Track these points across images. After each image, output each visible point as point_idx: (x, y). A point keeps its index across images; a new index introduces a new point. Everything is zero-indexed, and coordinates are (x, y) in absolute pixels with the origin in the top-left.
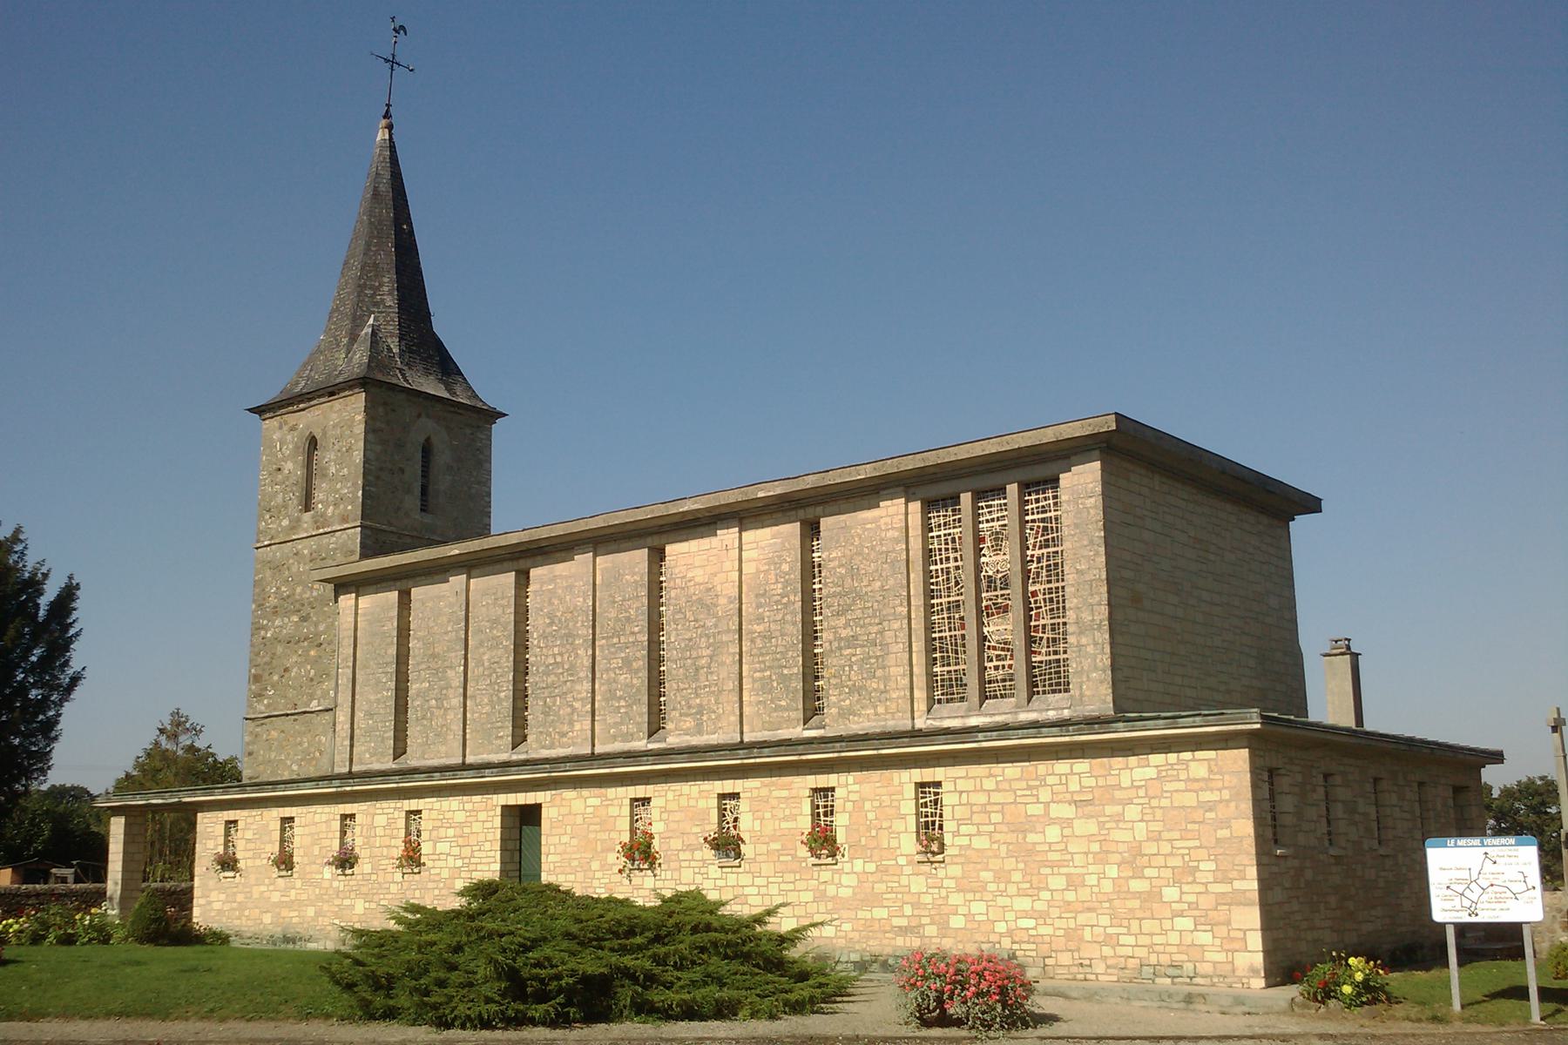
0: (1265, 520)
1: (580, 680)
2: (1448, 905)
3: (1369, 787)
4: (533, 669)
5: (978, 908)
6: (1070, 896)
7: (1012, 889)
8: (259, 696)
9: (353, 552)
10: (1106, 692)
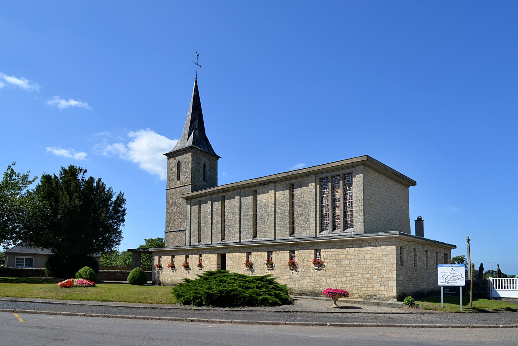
0: (402, 186)
1: (237, 224)
2: (442, 281)
3: (425, 253)
4: (226, 221)
5: (329, 280)
6: (351, 278)
7: (337, 276)
8: (168, 226)
10: (362, 228)
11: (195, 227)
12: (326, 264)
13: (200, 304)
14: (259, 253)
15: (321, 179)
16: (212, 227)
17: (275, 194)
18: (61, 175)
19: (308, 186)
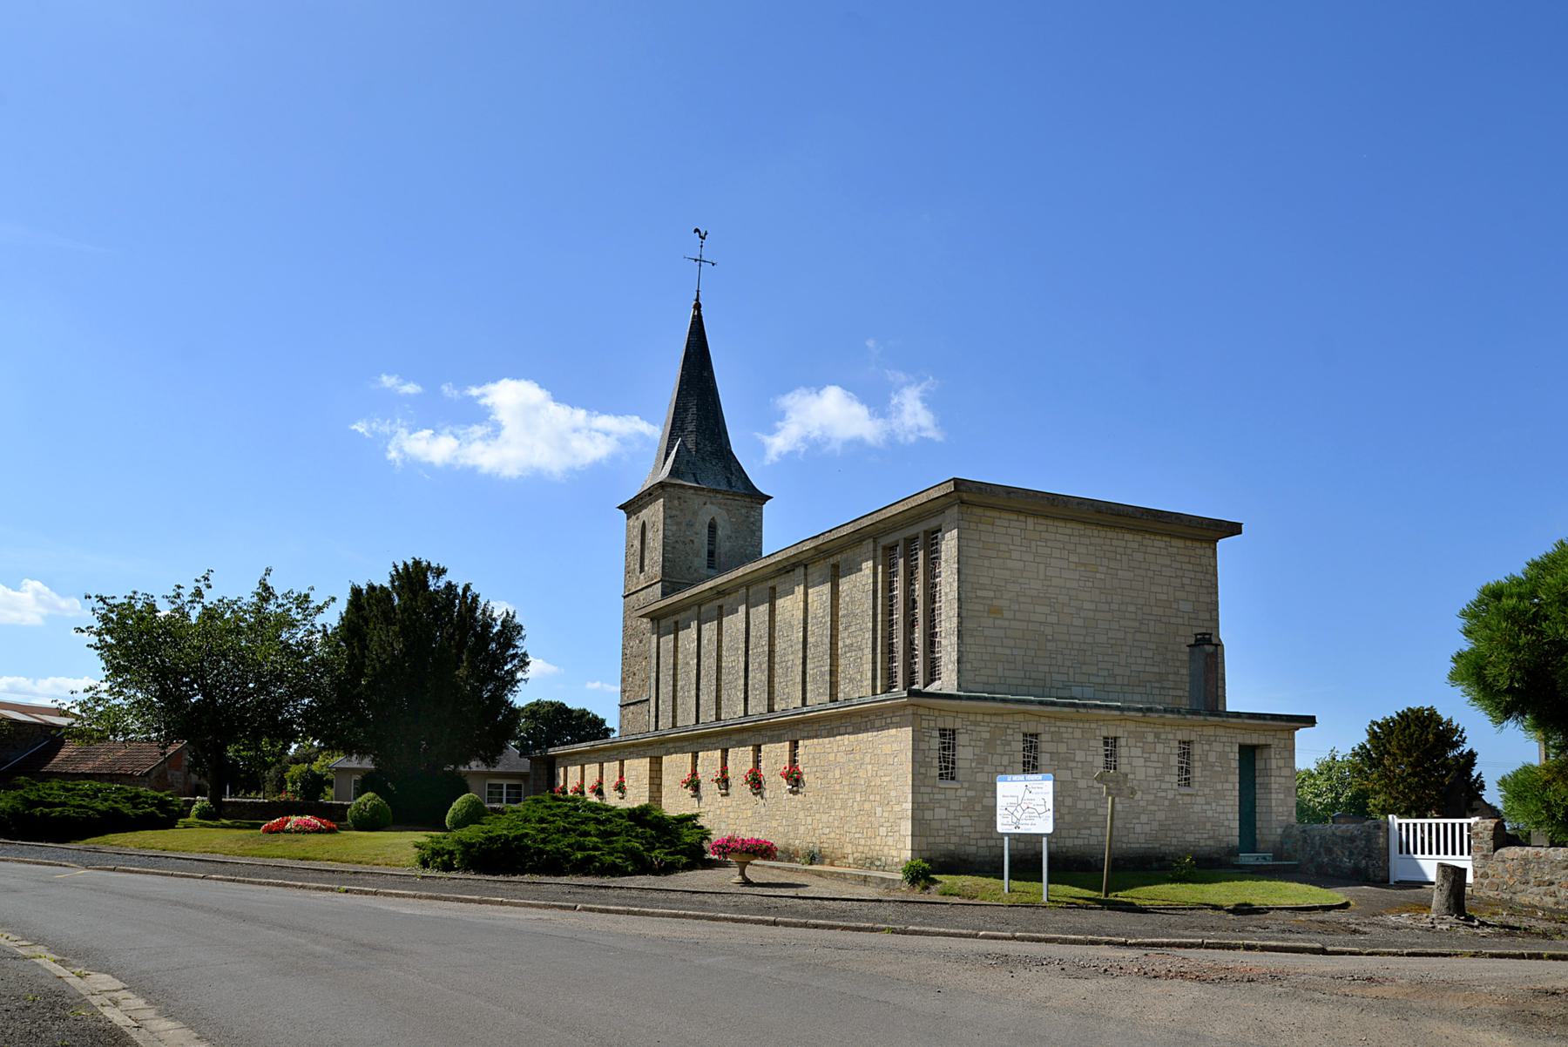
11: (666, 690)
13: (447, 867)
16: (698, 689)
17: (806, 594)
18: (392, 582)
19: (135, 639)
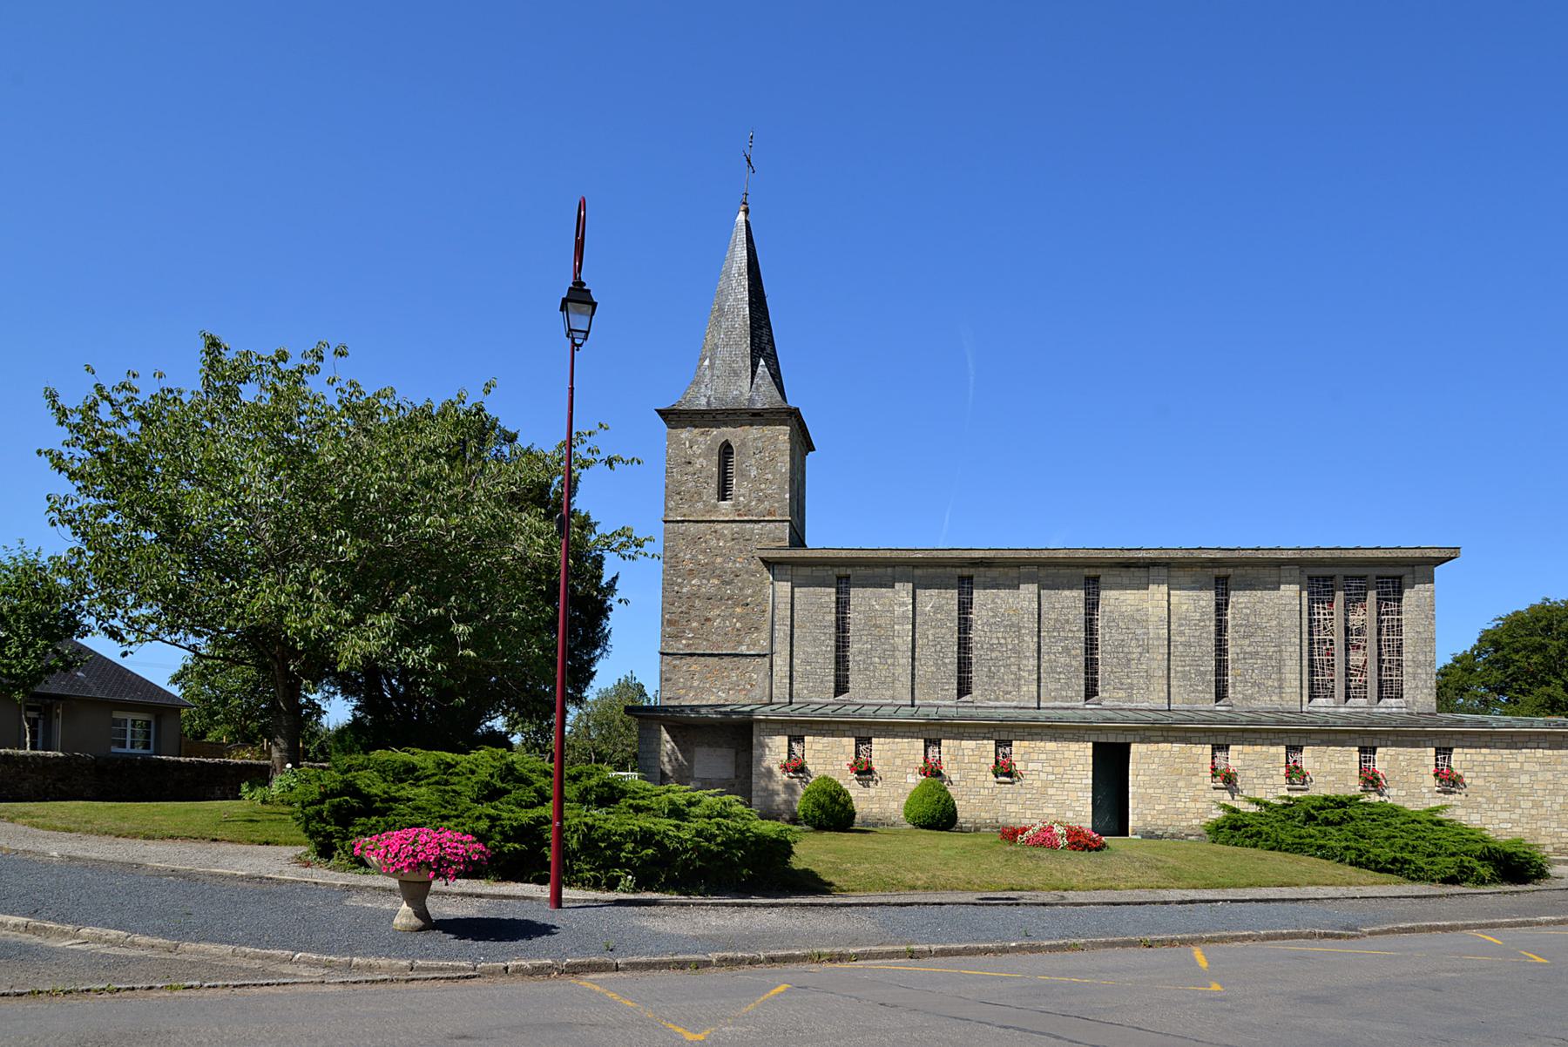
6: (1533, 812)
8: (676, 637)
9: (781, 540)
12: (1467, 781)
14: (1258, 748)
15: (1310, 578)
